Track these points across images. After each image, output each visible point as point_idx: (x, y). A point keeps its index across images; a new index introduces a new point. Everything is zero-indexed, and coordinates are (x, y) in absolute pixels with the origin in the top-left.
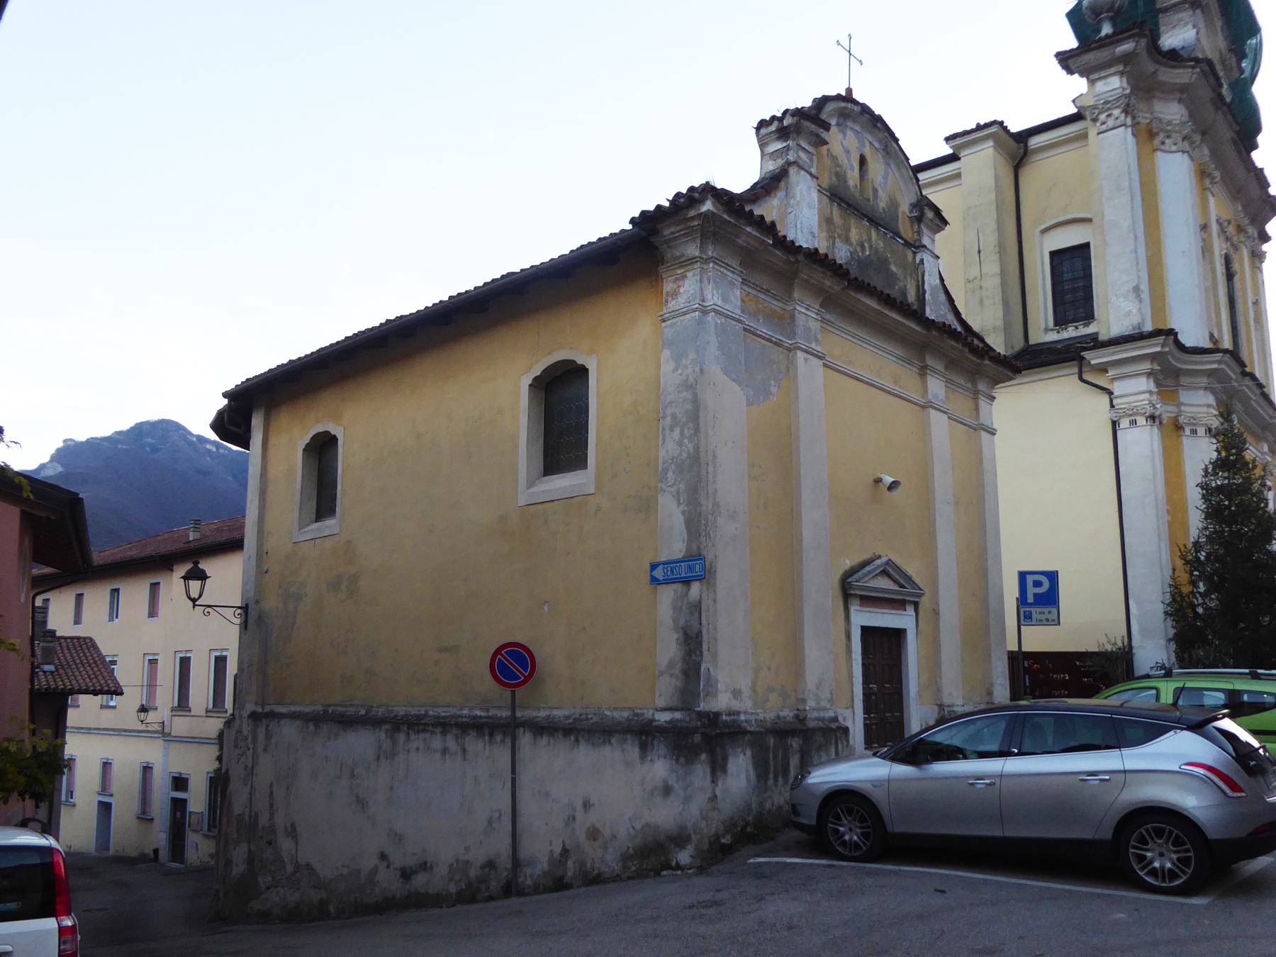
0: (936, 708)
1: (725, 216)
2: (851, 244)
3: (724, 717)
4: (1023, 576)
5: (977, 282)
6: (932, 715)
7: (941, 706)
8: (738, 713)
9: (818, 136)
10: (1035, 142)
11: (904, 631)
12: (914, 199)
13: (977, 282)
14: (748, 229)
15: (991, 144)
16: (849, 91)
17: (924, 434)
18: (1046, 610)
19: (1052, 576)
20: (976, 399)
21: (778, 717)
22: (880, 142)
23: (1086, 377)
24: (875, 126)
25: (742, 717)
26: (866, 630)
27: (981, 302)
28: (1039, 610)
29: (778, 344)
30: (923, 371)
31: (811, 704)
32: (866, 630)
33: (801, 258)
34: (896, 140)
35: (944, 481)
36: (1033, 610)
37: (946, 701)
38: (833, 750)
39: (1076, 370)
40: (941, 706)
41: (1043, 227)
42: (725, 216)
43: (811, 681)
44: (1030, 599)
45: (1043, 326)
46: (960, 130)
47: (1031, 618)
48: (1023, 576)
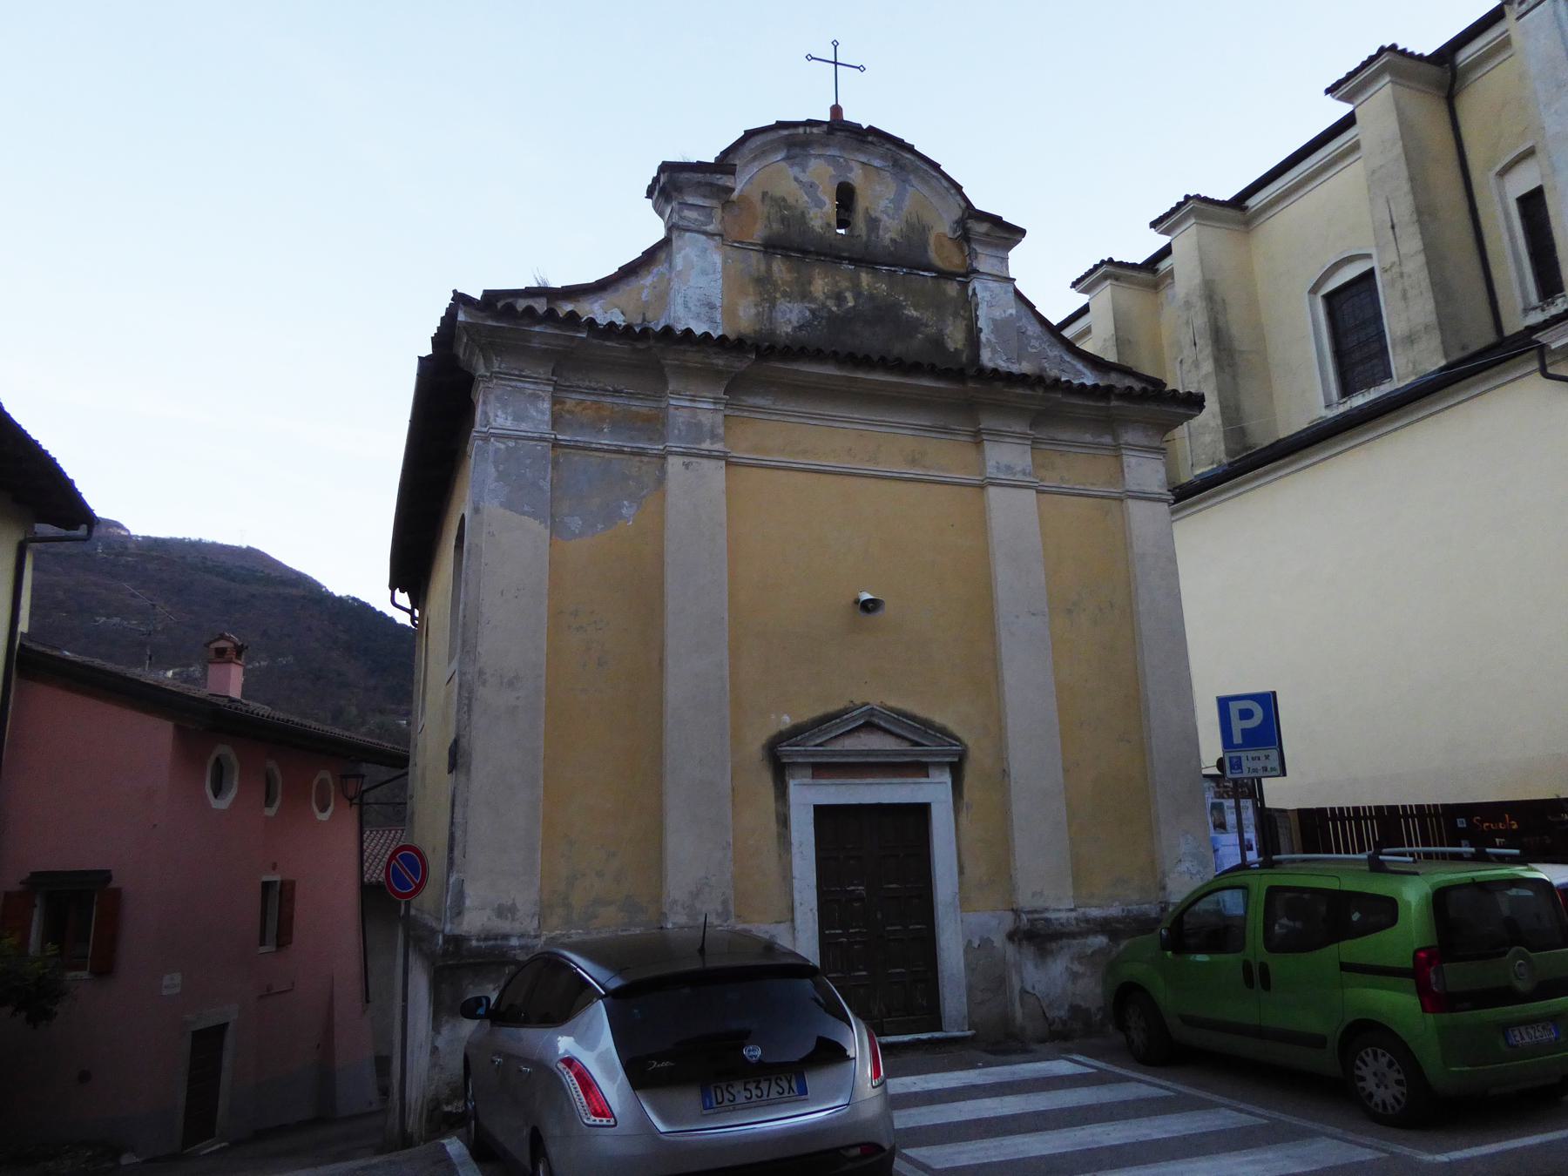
1: (490, 323)
2: (813, 300)
3: (474, 943)
4: (1224, 703)
5: (1395, 269)
6: (994, 923)
7: (1016, 912)
8: (506, 937)
9: (711, 185)
10: (1466, 55)
12: (956, 213)
13: (1395, 269)
14: (537, 329)
15: (1387, 78)
16: (836, 110)
17: (981, 524)
19: (1268, 701)
20: (1119, 457)
22: (882, 157)
23: (1550, 370)
24: (864, 142)
25: (514, 942)
26: (821, 812)
27: (1404, 297)
30: (977, 438)
32: (821, 812)
33: (652, 342)
34: (910, 149)
35: (14, 676)
36: (1243, 755)
37: (1025, 900)
39: (1536, 365)
40: (1016, 912)
41: (1498, 168)
42: (490, 323)
43: (678, 885)
45: (1520, 306)
46: (1342, 75)
47: (1240, 767)
48: (1224, 703)
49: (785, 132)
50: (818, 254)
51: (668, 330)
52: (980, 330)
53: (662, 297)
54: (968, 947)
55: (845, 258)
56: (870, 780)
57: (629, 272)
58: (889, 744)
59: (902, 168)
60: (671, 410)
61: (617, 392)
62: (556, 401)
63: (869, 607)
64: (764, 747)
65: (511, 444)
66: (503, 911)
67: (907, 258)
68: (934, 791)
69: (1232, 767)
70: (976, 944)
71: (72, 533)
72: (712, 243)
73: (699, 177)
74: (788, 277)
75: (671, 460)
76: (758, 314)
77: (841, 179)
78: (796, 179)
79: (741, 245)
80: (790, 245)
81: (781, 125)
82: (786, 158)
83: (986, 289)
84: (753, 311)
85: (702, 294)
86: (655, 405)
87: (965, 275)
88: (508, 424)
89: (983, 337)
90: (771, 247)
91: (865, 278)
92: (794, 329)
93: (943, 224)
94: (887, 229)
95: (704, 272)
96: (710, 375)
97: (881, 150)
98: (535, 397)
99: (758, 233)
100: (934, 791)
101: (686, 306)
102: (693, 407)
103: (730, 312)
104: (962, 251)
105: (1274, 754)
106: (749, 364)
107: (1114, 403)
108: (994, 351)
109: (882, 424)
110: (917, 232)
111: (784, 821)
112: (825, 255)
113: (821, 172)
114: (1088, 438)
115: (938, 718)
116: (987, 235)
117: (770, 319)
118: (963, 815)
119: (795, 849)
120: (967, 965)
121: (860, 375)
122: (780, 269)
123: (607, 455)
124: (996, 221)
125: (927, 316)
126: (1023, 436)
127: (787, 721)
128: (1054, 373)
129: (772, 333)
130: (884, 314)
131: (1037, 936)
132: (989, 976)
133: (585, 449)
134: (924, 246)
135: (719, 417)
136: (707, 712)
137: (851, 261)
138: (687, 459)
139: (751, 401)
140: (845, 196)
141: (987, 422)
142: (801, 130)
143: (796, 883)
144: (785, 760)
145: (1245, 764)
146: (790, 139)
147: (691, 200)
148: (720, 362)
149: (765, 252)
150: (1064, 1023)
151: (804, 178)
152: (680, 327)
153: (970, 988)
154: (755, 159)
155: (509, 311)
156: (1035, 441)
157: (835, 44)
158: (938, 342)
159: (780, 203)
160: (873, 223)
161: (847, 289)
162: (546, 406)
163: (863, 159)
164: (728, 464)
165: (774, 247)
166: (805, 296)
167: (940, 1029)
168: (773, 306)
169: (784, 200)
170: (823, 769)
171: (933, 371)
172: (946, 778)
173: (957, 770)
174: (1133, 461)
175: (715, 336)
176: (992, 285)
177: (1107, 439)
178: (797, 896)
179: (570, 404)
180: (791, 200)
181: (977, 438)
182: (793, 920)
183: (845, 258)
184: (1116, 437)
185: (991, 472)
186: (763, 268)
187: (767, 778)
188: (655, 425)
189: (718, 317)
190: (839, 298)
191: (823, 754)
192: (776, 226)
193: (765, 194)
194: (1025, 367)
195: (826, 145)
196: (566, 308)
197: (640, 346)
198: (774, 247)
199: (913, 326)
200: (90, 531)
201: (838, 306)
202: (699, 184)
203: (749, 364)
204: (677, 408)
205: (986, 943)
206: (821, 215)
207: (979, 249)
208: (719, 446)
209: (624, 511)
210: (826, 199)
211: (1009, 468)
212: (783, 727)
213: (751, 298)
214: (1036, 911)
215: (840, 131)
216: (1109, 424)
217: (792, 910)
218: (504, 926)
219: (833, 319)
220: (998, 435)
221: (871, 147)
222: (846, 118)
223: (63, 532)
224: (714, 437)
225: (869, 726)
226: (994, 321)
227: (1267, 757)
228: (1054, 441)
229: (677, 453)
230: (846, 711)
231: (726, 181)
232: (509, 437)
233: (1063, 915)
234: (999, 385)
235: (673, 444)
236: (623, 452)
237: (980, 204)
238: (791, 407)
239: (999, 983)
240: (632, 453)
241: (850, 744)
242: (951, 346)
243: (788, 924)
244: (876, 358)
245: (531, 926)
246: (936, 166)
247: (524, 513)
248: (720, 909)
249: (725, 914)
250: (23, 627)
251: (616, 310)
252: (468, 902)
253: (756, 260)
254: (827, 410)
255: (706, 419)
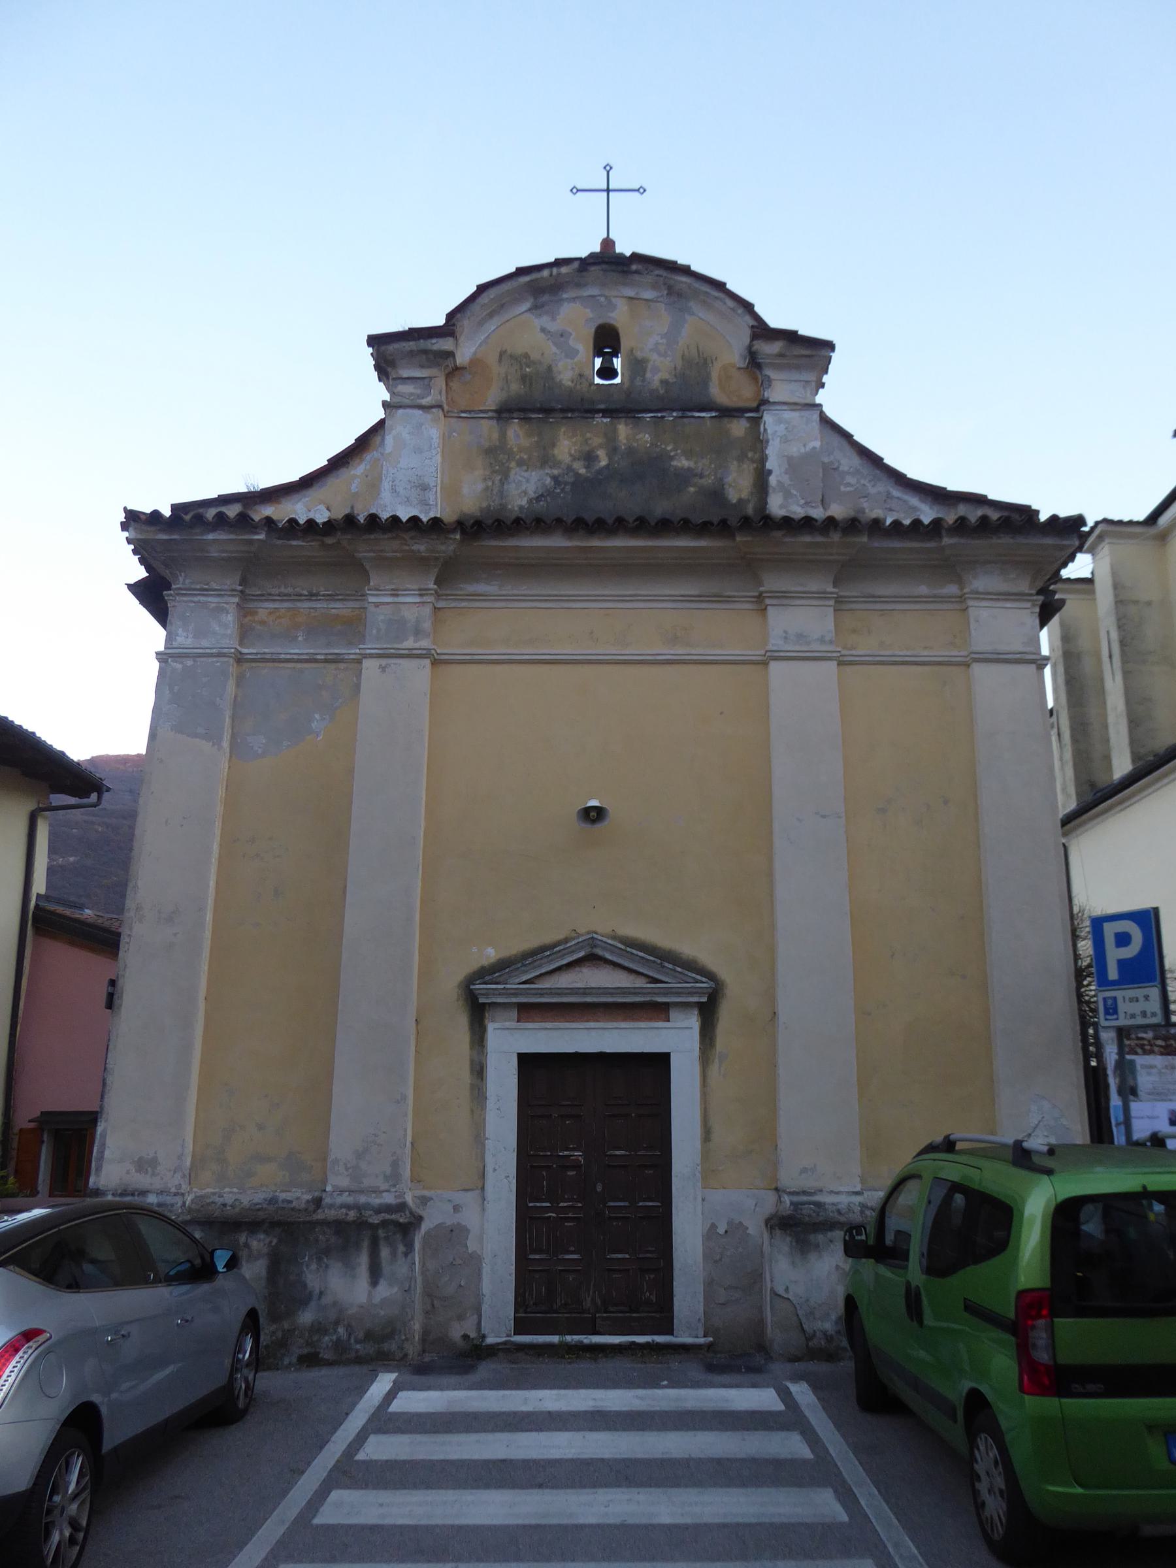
0: (774, 1192)
2: (556, 464)
3: (110, 1198)
6: (751, 1206)
8: (144, 1193)
9: (425, 352)
11: (663, 1060)
14: (210, 537)
16: (608, 243)
18: (1139, 993)
19: (1149, 920)
21: (272, 1201)
22: (655, 286)
26: (527, 1062)
28: (1130, 993)
29: (336, 660)
31: (338, 1180)
32: (527, 1062)
34: (686, 270)
36: (1119, 994)
37: (790, 1178)
38: (364, 1260)
42: (163, 536)
43: (341, 1146)
44: (1113, 974)
47: (1115, 1012)
49: (527, 279)
50: (562, 410)
51: (373, 518)
52: (770, 472)
53: (373, 486)
54: (711, 1233)
55: (598, 411)
56: (592, 1024)
57: (339, 462)
58: (621, 980)
59: (680, 295)
60: (371, 608)
61: (312, 595)
62: (244, 611)
63: (593, 815)
64: (459, 986)
65: (189, 663)
66: (145, 1165)
67: (685, 400)
68: (676, 1038)
69: (1107, 1012)
70: (721, 1231)
71: (85, 801)
72: (429, 416)
73: (411, 345)
74: (525, 442)
75: (366, 663)
76: (487, 489)
77: (600, 321)
78: (543, 330)
79: (471, 414)
80: (538, 405)
81: (521, 271)
82: (535, 308)
83: (780, 421)
84: (480, 486)
85: (423, 478)
86: (357, 605)
87: (757, 410)
88: (189, 642)
89: (773, 480)
90: (505, 412)
91: (623, 430)
92: (530, 501)
93: (730, 349)
94: (656, 370)
95: (418, 450)
96: (421, 563)
97: (649, 279)
98: (220, 610)
99: (493, 398)
100: (676, 1038)
101: (394, 490)
102: (397, 601)
103: (451, 491)
104: (755, 379)
105: (1154, 993)
106: (466, 547)
107: (947, 541)
108: (787, 495)
109: (633, 598)
110: (697, 367)
111: (479, 1071)
112: (572, 411)
113: (575, 318)
114: (923, 590)
115: (687, 949)
116: (781, 355)
117: (501, 494)
118: (714, 1069)
119: (490, 1104)
120: (706, 1256)
121: (596, 542)
122: (517, 434)
123: (299, 665)
124: (791, 337)
125: (701, 463)
126: (822, 596)
127: (491, 955)
128: (877, 513)
129: (503, 507)
130: (648, 468)
131: (798, 1225)
132: (739, 1274)
133: (274, 661)
134: (705, 382)
135: (428, 610)
136: (397, 946)
137: (606, 412)
138: (384, 662)
139: (471, 588)
140: (607, 340)
141: (772, 582)
142: (546, 273)
143: (489, 1144)
144: (481, 1000)
145: (1122, 1007)
146: (538, 284)
147: (405, 373)
148: (421, 547)
149: (499, 419)
150: (829, 1338)
151: (553, 327)
152: (385, 515)
153: (709, 1284)
154: (491, 315)
155: (199, 520)
156: (839, 600)
157: (608, 169)
158: (716, 494)
159: (521, 360)
160: (637, 366)
161: (600, 446)
162: (230, 618)
163: (630, 292)
164: (435, 663)
165: (510, 411)
166: (546, 460)
167: (670, 1332)
168: (505, 475)
169: (526, 356)
170: (528, 1011)
171: (703, 529)
172: (693, 1022)
173: (708, 1011)
174: (984, 614)
175: (425, 519)
176: (788, 415)
177: (952, 589)
178: (489, 1160)
179: (262, 614)
180: (535, 356)
181: (760, 603)
182: (483, 1188)
183: (598, 411)
184: (961, 583)
185: (775, 642)
186: (496, 435)
187: (462, 1020)
188: (354, 627)
189: (431, 496)
190: (589, 458)
191: (525, 993)
192: (515, 387)
193: (502, 354)
194: (838, 510)
195: (579, 285)
196: (268, 511)
197: (329, 541)
198: (510, 411)
199: (685, 477)
200: (99, 798)
201: (587, 467)
202: (412, 354)
203: (466, 547)
204: (377, 605)
205: (736, 1228)
206: (576, 366)
207: (768, 372)
208: (425, 643)
209: (314, 725)
210: (580, 347)
211: (800, 636)
212: (485, 962)
213: (479, 473)
214: (804, 1193)
215: (608, 263)
216: (950, 569)
217: (483, 1176)
218: (141, 1181)
219: (579, 484)
220: (783, 597)
221: (636, 277)
222: (618, 250)
223: (73, 800)
224: (418, 632)
225: (592, 959)
226: (790, 459)
227: (1147, 997)
228: (874, 598)
229: (371, 656)
230: (566, 940)
231: (446, 344)
232: (186, 656)
233: (843, 1200)
234: (778, 534)
235: (370, 646)
236: (316, 661)
237: (775, 321)
238: (523, 589)
239: (752, 1279)
240: (326, 661)
241: (565, 981)
242: (733, 496)
243: (478, 1192)
244: (610, 521)
245: (174, 1182)
246: (720, 286)
247: (196, 736)
248: (388, 1171)
249: (394, 1177)
250: (39, 886)
251: (322, 507)
252: (107, 1154)
253: (488, 429)
254: (567, 589)
255: (410, 614)
